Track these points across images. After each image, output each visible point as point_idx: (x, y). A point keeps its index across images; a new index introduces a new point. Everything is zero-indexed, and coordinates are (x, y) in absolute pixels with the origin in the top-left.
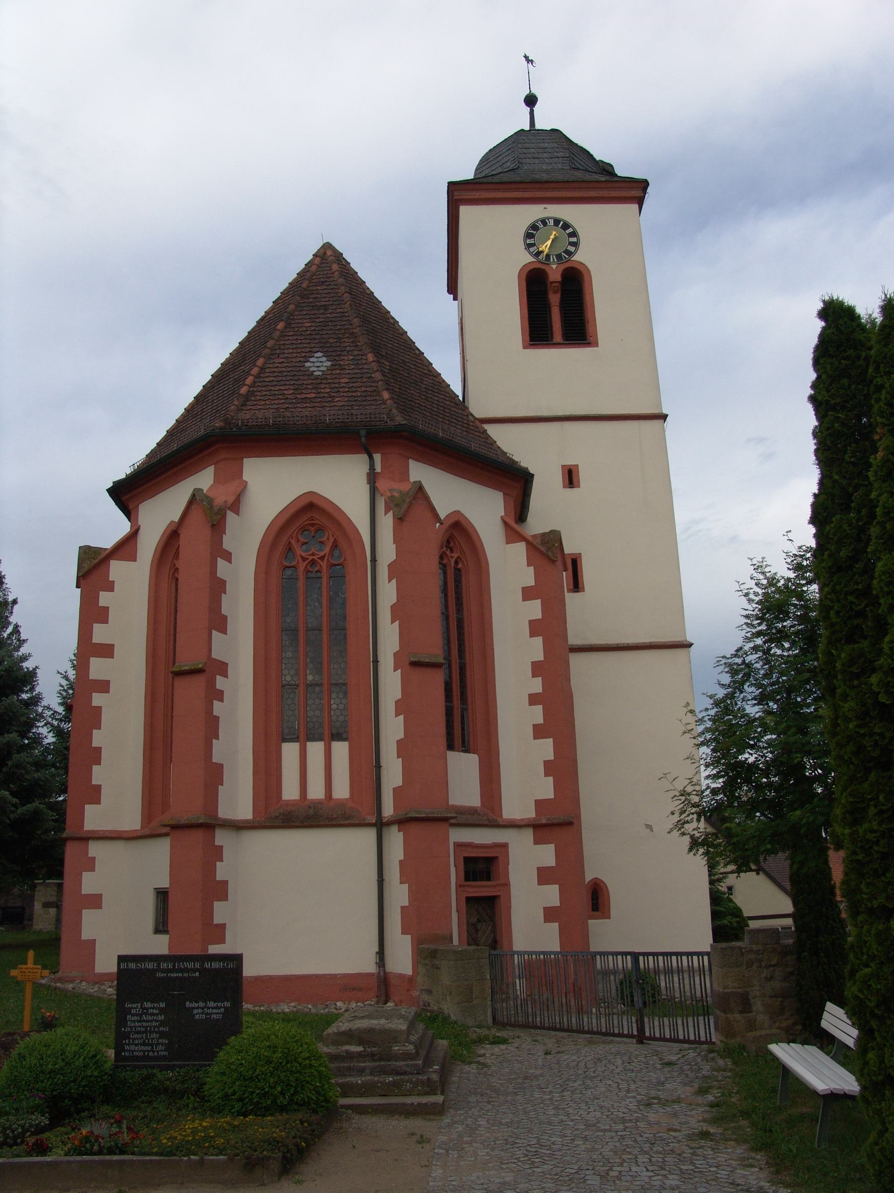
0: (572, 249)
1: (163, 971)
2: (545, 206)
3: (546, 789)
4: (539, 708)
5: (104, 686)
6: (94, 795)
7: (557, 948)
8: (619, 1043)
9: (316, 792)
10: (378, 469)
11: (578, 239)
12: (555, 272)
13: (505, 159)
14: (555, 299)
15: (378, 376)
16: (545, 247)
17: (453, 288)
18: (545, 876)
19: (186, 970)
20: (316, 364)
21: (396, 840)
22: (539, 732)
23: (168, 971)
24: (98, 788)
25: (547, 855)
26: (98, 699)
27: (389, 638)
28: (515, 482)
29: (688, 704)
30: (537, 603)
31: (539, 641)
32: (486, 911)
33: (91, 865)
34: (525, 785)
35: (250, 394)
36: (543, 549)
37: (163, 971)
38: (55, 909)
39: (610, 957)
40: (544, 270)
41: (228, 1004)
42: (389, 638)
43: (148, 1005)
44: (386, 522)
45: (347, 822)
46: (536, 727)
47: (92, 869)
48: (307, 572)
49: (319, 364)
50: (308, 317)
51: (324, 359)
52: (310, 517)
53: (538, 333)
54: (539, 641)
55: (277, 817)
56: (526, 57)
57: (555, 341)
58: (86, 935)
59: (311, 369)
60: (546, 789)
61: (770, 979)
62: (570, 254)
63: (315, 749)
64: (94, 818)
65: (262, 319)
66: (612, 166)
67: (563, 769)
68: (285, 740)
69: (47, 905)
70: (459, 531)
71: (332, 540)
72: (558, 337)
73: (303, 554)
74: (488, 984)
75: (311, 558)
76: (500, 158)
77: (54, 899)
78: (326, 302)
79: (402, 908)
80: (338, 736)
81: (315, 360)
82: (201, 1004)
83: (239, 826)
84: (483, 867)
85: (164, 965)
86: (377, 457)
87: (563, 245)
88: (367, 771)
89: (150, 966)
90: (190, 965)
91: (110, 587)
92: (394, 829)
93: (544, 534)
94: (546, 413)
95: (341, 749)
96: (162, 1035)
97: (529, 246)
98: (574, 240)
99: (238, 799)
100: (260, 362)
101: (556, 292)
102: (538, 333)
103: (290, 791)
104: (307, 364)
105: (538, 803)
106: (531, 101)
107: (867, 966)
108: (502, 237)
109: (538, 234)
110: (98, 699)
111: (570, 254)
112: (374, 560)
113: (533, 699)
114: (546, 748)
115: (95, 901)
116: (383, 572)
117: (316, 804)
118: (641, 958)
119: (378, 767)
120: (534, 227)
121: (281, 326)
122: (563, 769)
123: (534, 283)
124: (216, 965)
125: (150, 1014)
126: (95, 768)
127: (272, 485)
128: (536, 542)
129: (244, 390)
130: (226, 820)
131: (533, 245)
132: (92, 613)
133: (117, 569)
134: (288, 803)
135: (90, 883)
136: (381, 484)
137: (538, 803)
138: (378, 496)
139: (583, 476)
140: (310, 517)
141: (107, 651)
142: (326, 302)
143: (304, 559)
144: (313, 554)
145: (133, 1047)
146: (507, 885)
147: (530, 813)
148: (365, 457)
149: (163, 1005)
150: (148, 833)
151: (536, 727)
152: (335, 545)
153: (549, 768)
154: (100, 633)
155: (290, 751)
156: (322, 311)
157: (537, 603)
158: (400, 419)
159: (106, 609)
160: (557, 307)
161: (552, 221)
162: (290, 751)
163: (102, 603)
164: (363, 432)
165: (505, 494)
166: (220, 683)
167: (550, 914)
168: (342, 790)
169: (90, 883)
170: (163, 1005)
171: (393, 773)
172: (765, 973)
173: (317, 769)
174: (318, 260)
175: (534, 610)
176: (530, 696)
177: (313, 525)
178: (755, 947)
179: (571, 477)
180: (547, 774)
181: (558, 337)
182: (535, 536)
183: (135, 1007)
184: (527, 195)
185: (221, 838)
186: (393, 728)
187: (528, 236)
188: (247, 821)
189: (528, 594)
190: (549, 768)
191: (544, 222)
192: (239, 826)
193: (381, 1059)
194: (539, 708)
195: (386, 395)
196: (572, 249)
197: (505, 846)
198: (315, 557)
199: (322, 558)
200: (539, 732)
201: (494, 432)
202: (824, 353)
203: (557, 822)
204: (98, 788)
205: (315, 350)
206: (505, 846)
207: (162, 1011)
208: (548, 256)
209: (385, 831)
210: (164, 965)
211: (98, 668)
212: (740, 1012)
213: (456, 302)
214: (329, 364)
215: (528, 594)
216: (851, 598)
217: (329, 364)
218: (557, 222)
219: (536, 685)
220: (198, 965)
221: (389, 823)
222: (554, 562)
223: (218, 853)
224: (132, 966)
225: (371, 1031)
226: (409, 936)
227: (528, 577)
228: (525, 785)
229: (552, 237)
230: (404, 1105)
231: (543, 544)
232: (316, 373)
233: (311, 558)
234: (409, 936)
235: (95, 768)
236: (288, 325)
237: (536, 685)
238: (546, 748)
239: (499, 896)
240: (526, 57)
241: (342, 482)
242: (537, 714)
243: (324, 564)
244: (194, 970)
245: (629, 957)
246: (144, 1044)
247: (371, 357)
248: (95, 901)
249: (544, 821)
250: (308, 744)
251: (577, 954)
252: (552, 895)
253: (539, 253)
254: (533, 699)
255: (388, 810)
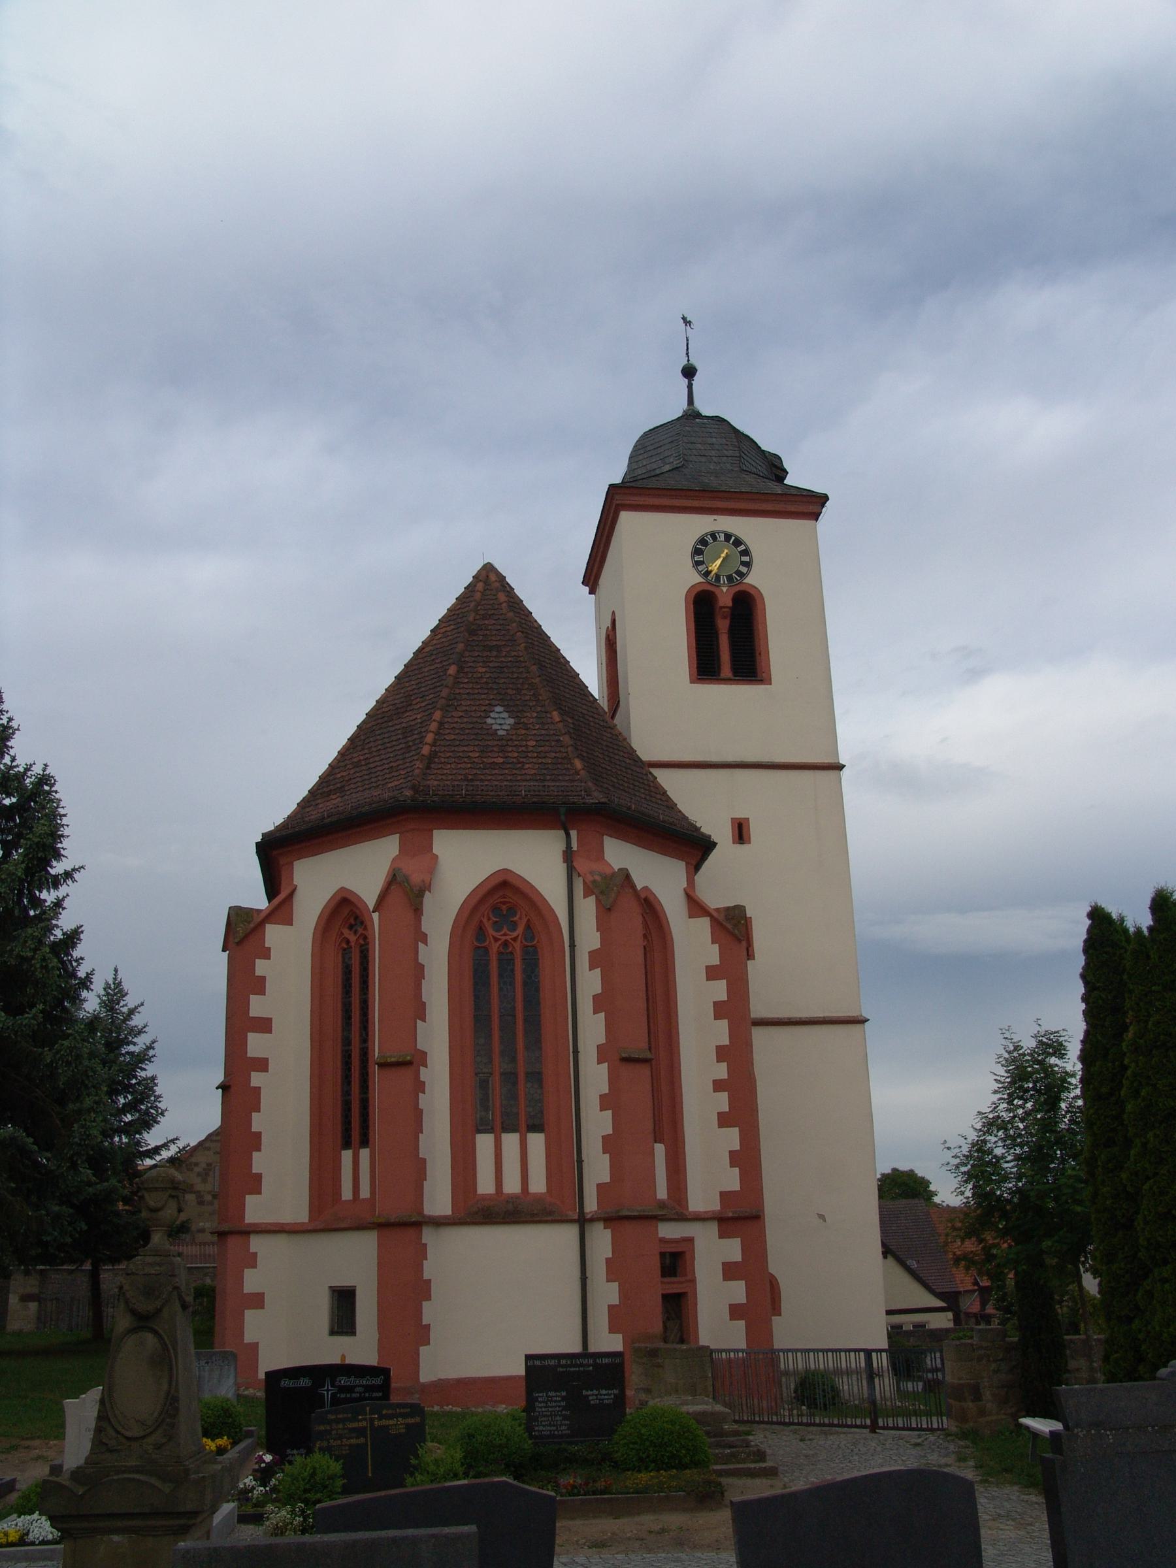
0: (744, 569)
1: (562, 1366)
2: (715, 517)
3: (732, 1181)
4: (724, 1096)
5: (262, 1065)
6: (255, 1184)
7: (744, 1346)
8: (837, 1433)
9: (512, 1186)
10: (575, 847)
11: (751, 559)
12: (725, 595)
13: (666, 454)
14: (723, 625)
15: (566, 739)
16: (715, 566)
17: (591, 579)
18: (730, 1271)
19: (582, 1365)
20: (499, 721)
21: (602, 1241)
22: (724, 1120)
23: (566, 1366)
24: (259, 1177)
25: (733, 1250)
26: (256, 1079)
27: (592, 1030)
28: (693, 847)
29: (945, 1142)
30: (723, 984)
31: (724, 1024)
32: (678, 1307)
33: (252, 1261)
34: (709, 1177)
35: (433, 756)
36: (729, 926)
37: (562, 1366)
38: (36, 1304)
39: (811, 1354)
40: (713, 593)
41: (616, 1392)
42: (592, 1030)
43: (552, 1394)
44: (587, 908)
45: (550, 1218)
46: (720, 1115)
47: (254, 1266)
48: (500, 953)
49: (500, 720)
50: (480, 659)
51: (505, 715)
52: (504, 897)
53: (706, 668)
54: (724, 1024)
55: (476, 1213)
56: (684, 318)
57: (722, 676)
58: (249, 1338)
59: (495, 727)
60: (732, 1181)
61: (996, 1372)
62: (742, 575)
63: (511, 1141)
64: (255, 1210)
65: (420, 650)
66: (780, 458)
67: (747, 1159)
68: (480, 1132)
69: (25, 1298)
70: (649, 907)
71: (525, 920)
72: (726, 671)
73: (495, 934)
74: (710, 1382)
75: (504, 938)
76: (659, 451)
77: (35, 1290)
78: (487, 627)
79: (611, 1307)
80: (536, 1127)
81: (496, 716)
82: (595, 1392)
83: (439, 1223)
84: (675, 1261)
85: (563, 1362)
86: (574, 834)
87: (735, 565)
88: (566, 1163)
89: (552, 1362)
90: (585, 1362)
91: (266, 954)
92: (600, 1226)
93: (728, 909)
94: (714, 758)
95: (537, 1141)
96: (565, 1418)
97: (697, 564)
98: (746, 559)
99: (439, 1197)
100: (438, 715)
101: (725, 618)
102: (706, 668)
103: (485, 1185)
104: (489, 721)
105: (723, 1195)
106: (689, 372)
107: (1116, 1352)
108: (665, 549)
109: (707, 550)
110: (256, 1079)
111: (739, 573)
112: (572, 946)
113: (718, 1086)
114: (732, 1138)
115: (258, 1300)
116: (583, 961)
117: (512, 1198)
118: (874, 1354)
119: (580, 1162)
120: (703, 541)
121: (452, 670)
122: (747, 1159)
123: (702, 605)
124: (606, 1361)
125: (552, 1402)
126: (255, 1154)
127: (464, 861)
128: (721, 918)
129: (426, 750)
130: (430, 1217)
131: (702, 563)
132: (243, 983)
133: (274, 934)
134: (484, 1197)
135: (252, 1281)
136: (580, 864)
137: (723, 1195)
138: (575, 876)
139: (754, 830)
140: (504, 897)
141: (264, 1025)
142: (487, 627)
143: (496, 940)
144: (505, 935)
145: (541, 1428)
146: (693, 1281)
147: (715, 1206)
148: (562, 833)
149: (564, 1394)
150: (321, 1227)
151: (720, 1115)
152: (528, 926)
153: (735, 1158)
154: (257, 1007)
155: (484, 1143)
156: (495, 653)
157: (723, 984)
158: (598, 797)
159: (263, 979)
160: (728, 636)
161: (722, 535)
162: (484, 1143)
163: (258, 972)
164: (563, 810)
165: (687, 864)
166: (424, 1074)
167: (736, 1312)
168: (538, 1184)
169: (252, 1281)
170: (564, 1394)
171: (598, 1168)
172: (993, 1366)
173: (514, 1162)
174: (480, 586)
175: (719, 990)
176: (715, 1082)
177: (504, 903)
178: (984, 1344)
179: (741, 832)
180: (732, 1165)
181: (726, 671)
182: (717, 910)
183: (542, 1396)
184: (696, 503)
185: (428, 1236)
186: (597, 1124)
187: (697, 551)
188: (446, 1217)
189: (712, 973)
190: (735, 1158)
191: (714, 536)
192: (439, 1223)
193: (715, 1436)
194: (724, 1096)
195: (578, 764)
196: (744, 569)
197: (690, 1240)
198: (508, 938)
199: (515, 939)
200: (724, 1120)
201: (666, 779)
202: (1091, 946)
203: (742, 1216)
204: (259, 1177)
205: (493, 702)
206: (690, 1240)
207: (563, 1398)
208: (718, 577)
209: (587, 1227)
210: (563, 1362)
211: (256, 1045)
212: (973, 1401)
213: (593, 596)
214: (512, 721)
215: (712, 973)
216: (1108, 1120)
217: (512, 721)
218: (728, 536)
219: (721, 1071)
220: (591, 1361)
221: (592, 1220)
222: (740, 941)
223: (421, 1252)
224: (538, 1363)
225: (704, 1413)
226: (620, 1336)
227: (713, 955)
228: (709, 1177)
229: (723, 555)
230: (750, 1469)
231: (727, 919)
232: (500, 733)
233: (504, 938)
234: (620, 1336)
235: (255, 1154)
236: (461, 669)
237: (721, 1071)
238: (732, 1138)
239: (685, 1293)
240: (684, 318)
241: (536, 859)
242: (722, 1101)
243: (517, 945)
244: (589, 1366)
245: (862, 1354)
246: (550, 1425)
247: (556, 715)
248: (258, 1300)
249: (730, 1215)
250: (504, 1136)
251: (761, 1352)
252: (738, 1291)
253: (708, 573)
254: (718, 1086)
255: (591, 1205)
